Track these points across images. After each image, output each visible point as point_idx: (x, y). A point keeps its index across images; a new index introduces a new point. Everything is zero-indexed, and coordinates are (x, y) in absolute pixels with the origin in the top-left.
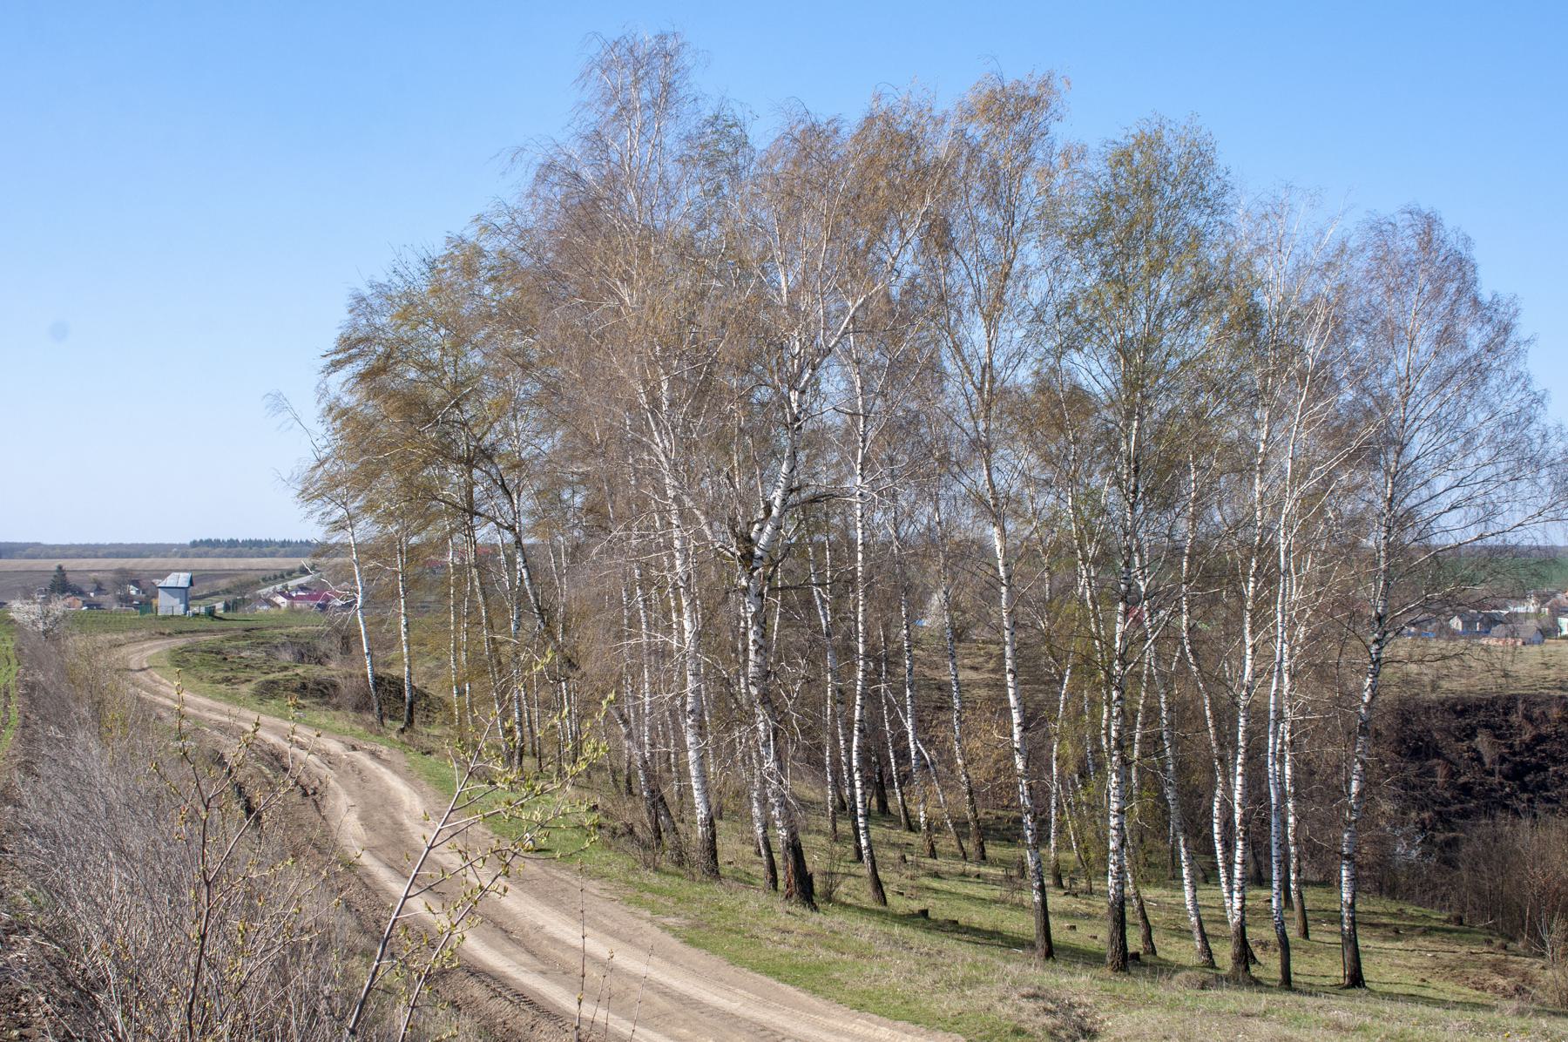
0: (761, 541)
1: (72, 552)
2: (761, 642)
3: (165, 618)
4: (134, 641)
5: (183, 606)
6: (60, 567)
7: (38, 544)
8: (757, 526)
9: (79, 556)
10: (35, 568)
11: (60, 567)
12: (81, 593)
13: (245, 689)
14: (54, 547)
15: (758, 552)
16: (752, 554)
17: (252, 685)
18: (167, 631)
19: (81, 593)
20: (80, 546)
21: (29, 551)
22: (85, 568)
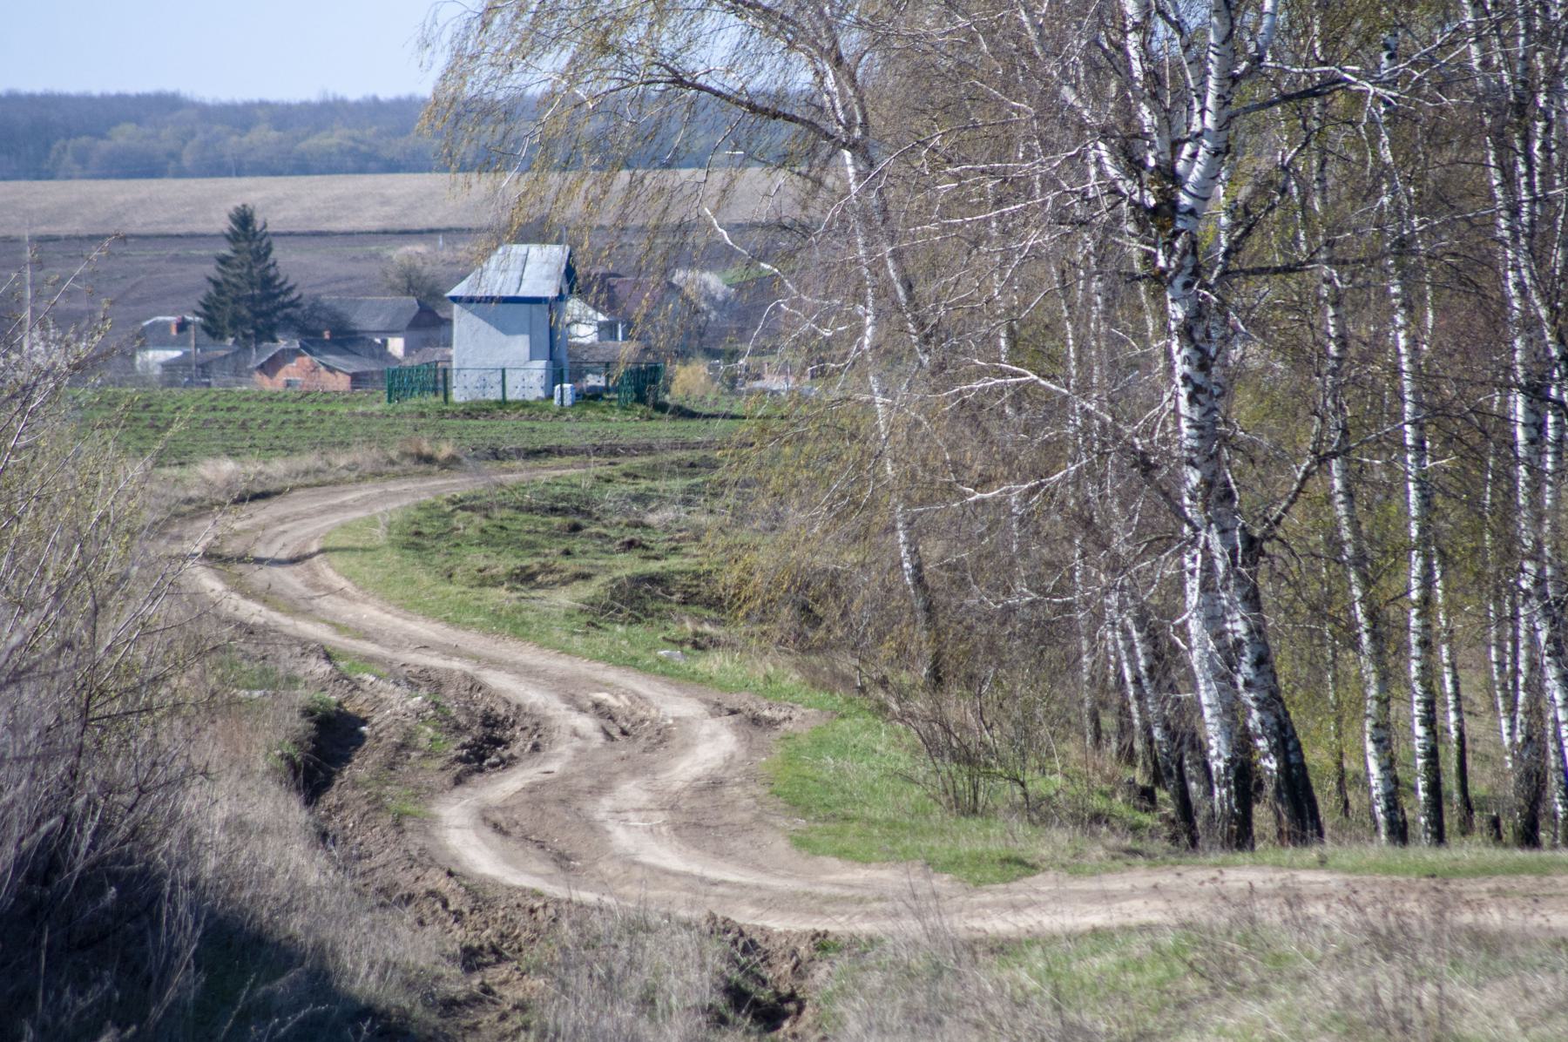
0: (1191, 178)
1: (331, 139)
2: (1199, 378)
3: (472, 411)
4: (317, 481)
5: (540, 365)
6: (244, 219)
7: (165, 105)
8: (1188, 149)
9: (363, 161)
10: (138, 223)
11: (244, 219)
12: (345, 338)
13: (563, 598)
14: (242, 116)
15: (1185, 200)
16: (1174, 205)
17: (587, 591)
18: (445, 450)
19: (345, 338)
20: (374, 109)
21: (124, 136)
22: (369, 219)
